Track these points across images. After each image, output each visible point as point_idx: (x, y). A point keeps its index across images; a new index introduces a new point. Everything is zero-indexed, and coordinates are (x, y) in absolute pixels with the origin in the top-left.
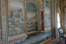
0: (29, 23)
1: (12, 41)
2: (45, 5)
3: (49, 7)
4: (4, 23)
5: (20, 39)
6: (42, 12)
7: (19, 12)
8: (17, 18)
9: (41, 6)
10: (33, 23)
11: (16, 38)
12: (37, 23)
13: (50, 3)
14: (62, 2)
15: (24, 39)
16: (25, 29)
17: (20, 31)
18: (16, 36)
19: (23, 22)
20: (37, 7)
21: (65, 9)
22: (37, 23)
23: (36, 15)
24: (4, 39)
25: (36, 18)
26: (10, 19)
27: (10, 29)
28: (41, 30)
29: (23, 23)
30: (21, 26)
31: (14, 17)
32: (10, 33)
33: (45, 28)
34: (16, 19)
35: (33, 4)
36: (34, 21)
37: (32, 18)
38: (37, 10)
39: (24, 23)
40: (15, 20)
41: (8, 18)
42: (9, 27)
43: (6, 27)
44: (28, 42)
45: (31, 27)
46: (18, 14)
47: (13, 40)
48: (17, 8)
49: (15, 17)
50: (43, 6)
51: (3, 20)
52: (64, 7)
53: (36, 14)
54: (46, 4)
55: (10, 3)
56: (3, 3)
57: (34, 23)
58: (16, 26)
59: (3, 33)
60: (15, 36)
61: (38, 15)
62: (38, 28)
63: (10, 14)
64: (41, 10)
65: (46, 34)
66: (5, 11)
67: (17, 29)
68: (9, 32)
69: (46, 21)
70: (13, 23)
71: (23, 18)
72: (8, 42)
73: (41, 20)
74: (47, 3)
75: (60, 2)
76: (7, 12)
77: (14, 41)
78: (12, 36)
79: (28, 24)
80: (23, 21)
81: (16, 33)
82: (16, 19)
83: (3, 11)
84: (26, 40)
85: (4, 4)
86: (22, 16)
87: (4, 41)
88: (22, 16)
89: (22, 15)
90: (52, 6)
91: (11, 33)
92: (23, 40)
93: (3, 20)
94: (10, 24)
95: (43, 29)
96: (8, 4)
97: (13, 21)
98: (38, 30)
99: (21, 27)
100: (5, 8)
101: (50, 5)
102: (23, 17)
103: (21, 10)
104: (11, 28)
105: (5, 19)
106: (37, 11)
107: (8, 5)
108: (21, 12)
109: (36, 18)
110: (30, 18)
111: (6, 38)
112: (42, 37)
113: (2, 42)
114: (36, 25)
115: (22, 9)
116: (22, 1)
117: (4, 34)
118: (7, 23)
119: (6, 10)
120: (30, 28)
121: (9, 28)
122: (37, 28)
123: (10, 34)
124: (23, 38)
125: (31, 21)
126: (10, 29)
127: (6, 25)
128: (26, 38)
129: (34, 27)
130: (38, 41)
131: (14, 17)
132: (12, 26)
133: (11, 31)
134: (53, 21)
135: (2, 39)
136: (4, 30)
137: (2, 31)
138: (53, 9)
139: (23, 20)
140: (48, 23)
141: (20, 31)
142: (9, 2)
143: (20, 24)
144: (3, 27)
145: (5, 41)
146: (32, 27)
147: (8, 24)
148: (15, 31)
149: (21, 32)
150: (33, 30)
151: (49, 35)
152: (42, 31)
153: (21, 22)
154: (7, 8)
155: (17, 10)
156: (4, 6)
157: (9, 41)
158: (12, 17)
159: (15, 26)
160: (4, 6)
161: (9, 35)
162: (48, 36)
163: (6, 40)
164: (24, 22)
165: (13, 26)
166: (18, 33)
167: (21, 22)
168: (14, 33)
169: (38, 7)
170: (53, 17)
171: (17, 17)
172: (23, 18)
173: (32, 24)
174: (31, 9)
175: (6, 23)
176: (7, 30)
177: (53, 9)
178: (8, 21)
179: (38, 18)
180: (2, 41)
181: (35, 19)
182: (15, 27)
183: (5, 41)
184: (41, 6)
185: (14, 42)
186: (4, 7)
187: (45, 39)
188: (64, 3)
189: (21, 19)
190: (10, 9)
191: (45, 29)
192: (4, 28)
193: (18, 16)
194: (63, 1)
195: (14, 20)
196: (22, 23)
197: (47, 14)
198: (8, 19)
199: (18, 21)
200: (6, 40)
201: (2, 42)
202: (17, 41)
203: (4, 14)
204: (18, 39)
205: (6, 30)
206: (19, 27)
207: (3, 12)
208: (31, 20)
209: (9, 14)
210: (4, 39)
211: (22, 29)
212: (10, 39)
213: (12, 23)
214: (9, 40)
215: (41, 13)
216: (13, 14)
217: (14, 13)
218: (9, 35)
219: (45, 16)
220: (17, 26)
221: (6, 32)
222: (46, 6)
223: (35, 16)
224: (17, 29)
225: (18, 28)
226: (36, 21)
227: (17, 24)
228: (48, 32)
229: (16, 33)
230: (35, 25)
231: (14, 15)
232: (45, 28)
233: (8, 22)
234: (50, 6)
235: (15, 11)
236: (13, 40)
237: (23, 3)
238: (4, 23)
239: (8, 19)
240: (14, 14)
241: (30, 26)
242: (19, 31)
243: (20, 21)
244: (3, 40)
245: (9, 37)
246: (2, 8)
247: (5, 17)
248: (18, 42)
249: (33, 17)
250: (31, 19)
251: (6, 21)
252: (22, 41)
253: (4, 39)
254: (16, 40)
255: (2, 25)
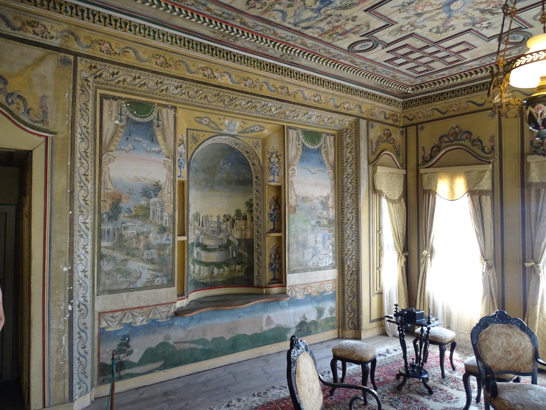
0: (210, 243)
1: (111, 314)
2: (293, 151)
3: (322, 163)
4: (82, 242)
5: (146, 309)
6: (279, 190)
7: (150, 197)
8: (139, 222)
9: (276, 160)
10: (229, 242)
11: (129, 304)
12: (249, 245)
13: (330, 140)
14: (412, 131)
15: (164, 315)
16: (173, 270)
17: (149, 276)
18: (128, 296)
19: (163, 239)
20: (253, 164)
21: (422, 171)
22: (249, 245)
23: (250, 205)
24: (82, 300)
25: (245, 218)
26: (107, 226)
27: (107, 267)
28: (269, 284)
29: (165, 245)
30: (155, 256)
31: (124, 220)
32: (107, 281)
33: (289, 276)
34: (133, 228)
35: (231, 149)
36: (237, 235)
37: (227, 218)
38: (254, 179)
39: (168, 242)
40: (129, 231)
41: (101, 220)
42: (101, 257)
43: (89, 257)
44: (184, 328)
45: (218, 265)
46: (142, 207)
47: (117, 311)
48: (139, 180)
49: (128, 219)
50: (282, 161)
51: (79, 232)
52: (420, 161)
53: (247, 199)
54: (305, 149)
55: (111, 165)
56: (82, 171)
57: (237, 243)
58: (131, 253)
59: (75, 278)
60: (124, 295)
61: (257, 205)
62: (256, 273)
63: (110, 205)
64: (273, 180)
65: (294, 302)
66: (89, 173)
67: (134, 265)
68: (103, 277)
69: (301, 238)
70: (120, 242)
71: (166, 221)
72: (97, 316)
73: (273, 231)
74: (314, 143)
75: (402, 133)
76: (99, 198)
77: (120, 317)
78: (111, 292)
79: (205, 248)
80: (165, 235)
81: (130, 283)
82: (133, 228)
83: (81, 198)
84: (172, 316)
85: (89, 173)
86: (158, 214)
87: (79, 306)
88: (158, 214)
89: (159, 209)
90: (348, 154)
91: (108, 282)
92: (158, 316)
93: (79, 232)
94: (105, 247)
95: (280, 279)
96: (105, 169)
97: (121, 236)
98: (256, 283)
99: (151, 261)
100: (90, 186)
101: (331, 151)
102: (166, 218)
103: (157, 188)
104: (109, 261)
105: (89, 226)
106: (251, 181)
107: (103, 173)
108: (156, 195)
109: (245, 218)
110: (215, 219)
111: (89, 299)
112: (269, 321)
113: (70, 309)
114: (246, 254)
115: (160, 184)
116: (164, 151)
117: (81, 282)
118: (93, 240)
119: (95, 194)
120: (216, 271)
121: (101, 262)
122: (250, 270)
123: (104, 284)
124: (161, 308)
125: (222, 235)
126: (107, 267)
127: (89, 248)
128: (172, 311)
129: (238, 267)
130: (240, 332)
131: (122, 217)
132: (116, 254)
133: (108, 273)
134: (346, 236)
135: (71, 297)
136: (81, 268)
137: (75, 270)
138: (349, 171)
139: (163, 230)
140: (315, 248)
141: (146, 275)
142: (110, 160)
143: (148, 247)
144: (79, 256)
145: (82, 307)
146: (227, 265)
147: (100, 247)
148: (127, 273)
149: (154, 281)
150: (229, 282)
151: (320, 312)
152: (275, 290)
153: (154, 238)
154: (100, 184)
155: (140, 190)
156: (87, 180)
157: (100, 314)
158: (116, 220)
159: (128, 254)
160: (87, 180)
161: (101, 288)
162: (312, 317)
163: (86, 304)
164: (168, 239)
165: (119, 255)
166: (139, 284)
167: (154, 238)
168: (122, 282)
169: (256, 162)
170: (349, 215)
171: (136, 216)
172: (166, 221)
173: (225, 247)
174: (225, 176)
175: (90, 243)
176: (93, 266)
177: (349, 171)
178: (99, 235)
179: (258, 218)
180: (72, 304)
181: (240, 223)
182: (126, 257)
183: (82, 307)
184: (273, 160)
185: (118, 319)
186: (86, 182)
187: (288, 330)
188: (421, 134)
189: (157, 228)
190: (109, 188)
191: (292, 279)
192: (81, 260)
193: (143, 214)
194: (416, 125)
195: (125, 228)
196: (159, 241)
197: (305, 199)
198: (100, 226)
199: (143, 233)
200: (89, 304)
201: (70, 309)
202: (132, 314)
203: (85, 210)
204: (138, 310)
205: (89, 269)
206: (142, 260)
207: (83, 203)
208: (219, 227)
209: (106, 208)
210: (82, 300)
211: (157, 267)
212: (103, 303)
213: (115, 241)
214: (98, 309)
215: (269, 195)
216: (121, 205)
217: (124, 201)
218: (101, 288)
219: (294, 210)
220: (133, 256)
221: (89, 274)
222: (302, 160)
223: (244, 210)
224: (134, 265)
225: (141, 264)
226: (248, 237)
227: (134, 245)
228: (310, 299)
229: (130, 283)
230: (240, 255)
231: (123, 211)
232: (294, 272)
233: (100, 238)
234: (332, 158)
235: (131, 192)
236: (117, 311)
237: (168, 157)
238: (82, 242)
239: (100, 226)
240: (125, 204)
241: (214, 257)
242: (143, 276)
243: (149, 233)
244: (77, 303)
245: (101, 297)
246: (80, 188)
247: (87, 221)
248: (138, 324)
249: (233, 214)
250: (219, 224)
251: (90, 233)
252: (154, 321)
253: (78, 299)
254: (128, 314)
255: (75, 250)
